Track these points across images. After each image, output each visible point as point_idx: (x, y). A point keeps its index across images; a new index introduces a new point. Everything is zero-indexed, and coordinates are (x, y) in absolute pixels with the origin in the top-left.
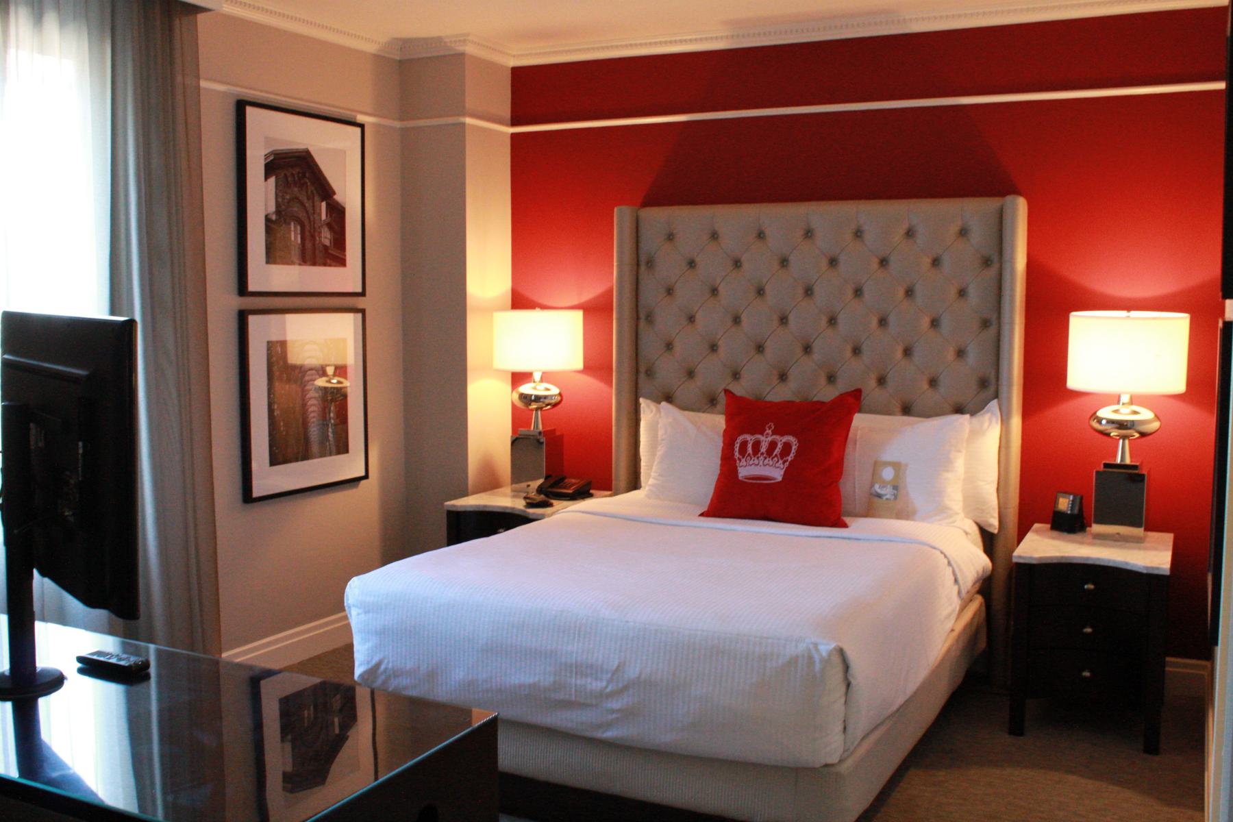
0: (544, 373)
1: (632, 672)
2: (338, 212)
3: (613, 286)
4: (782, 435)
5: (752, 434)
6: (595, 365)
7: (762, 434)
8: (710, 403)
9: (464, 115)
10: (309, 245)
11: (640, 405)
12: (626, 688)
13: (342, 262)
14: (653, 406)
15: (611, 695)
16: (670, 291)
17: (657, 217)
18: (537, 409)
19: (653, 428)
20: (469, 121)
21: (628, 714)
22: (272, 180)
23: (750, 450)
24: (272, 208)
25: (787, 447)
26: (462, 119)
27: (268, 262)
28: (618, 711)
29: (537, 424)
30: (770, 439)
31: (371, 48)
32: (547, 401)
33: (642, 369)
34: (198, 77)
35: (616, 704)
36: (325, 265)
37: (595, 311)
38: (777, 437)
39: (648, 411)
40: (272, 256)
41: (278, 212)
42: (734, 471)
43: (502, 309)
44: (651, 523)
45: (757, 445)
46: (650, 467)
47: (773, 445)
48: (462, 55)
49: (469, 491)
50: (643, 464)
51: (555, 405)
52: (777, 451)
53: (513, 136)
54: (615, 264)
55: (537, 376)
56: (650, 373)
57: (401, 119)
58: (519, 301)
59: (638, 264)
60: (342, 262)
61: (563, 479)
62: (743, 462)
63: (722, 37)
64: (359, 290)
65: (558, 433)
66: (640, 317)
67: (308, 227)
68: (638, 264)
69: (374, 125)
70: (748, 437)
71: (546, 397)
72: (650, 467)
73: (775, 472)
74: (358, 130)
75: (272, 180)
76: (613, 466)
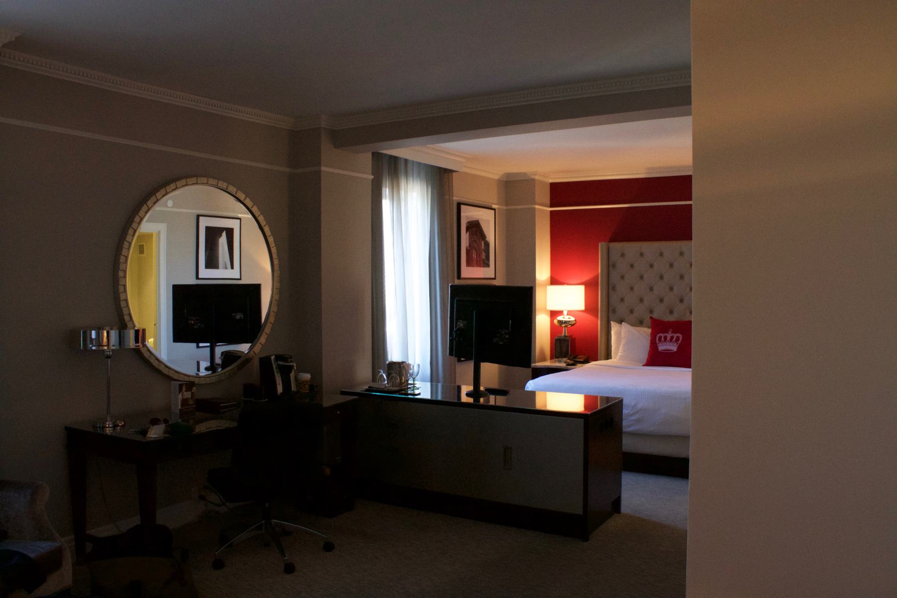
0: (568, 311)
1: (640, 406)
2: (487, 245)
3: (598, 275)
4: (676, 333)
5: (663, 333)
6: (591, 307)
7: (667, 333)
8: (640, 323)
9: (535, 204)
10: (478, 259)
11: (611, 324)
12: (637, 412)
13: (488, 265)
14: (617, 325)
15: (631, 415)
16: (623, 277)
17: (617, 246)
18: (565, 327)
19: (619, 334)
20: (537, 207)
21: (638, 421)
22: (468, 233)
23: (663, 339)
24: (468, 245)
25: (678, 338)
26: (534, 206)
27: (467, 266)
28: (634, 420)
29: (565, 332)
30: (671, 335)
31: (497, 177)
32: (570, 323)
33: (611, 309)
34: (453, 196)
35: (633, 418)
36: (484, 267)
37: (591, 286)
38: (674, 334)
39: (615, 328)
40: (469, 264)
41: (470, 246)
42: (657, 347)
43: (548, 285)
44: (628, 368)
45: (665, 338)
46: (617, 348)
47: (672, 338)
48: (534, 180)
49: (537, 361)
50: (613, 348)
51: (572, 325)
52: (674, 340)
53: (551, 212)
54: (600, 266)
55: (565, 313)
56: (614, 311)
57: (507, 205)
58: (554, 281)
59: (609, 266)
60: (488, 265)
61: (577, 355)
62: (660, 344)
63: (643, 173)
64: (493, 277)
65: (573, 337)
66: (610, 288)
67: (478, 252)
68: (609, 266)
69: (499, 209)
70: (662, 335)
71: (569, 321)
72: (617, 348)
73: (674, 348)
74: (493, 211)
75: (468, 233)
76: (599, 351)
